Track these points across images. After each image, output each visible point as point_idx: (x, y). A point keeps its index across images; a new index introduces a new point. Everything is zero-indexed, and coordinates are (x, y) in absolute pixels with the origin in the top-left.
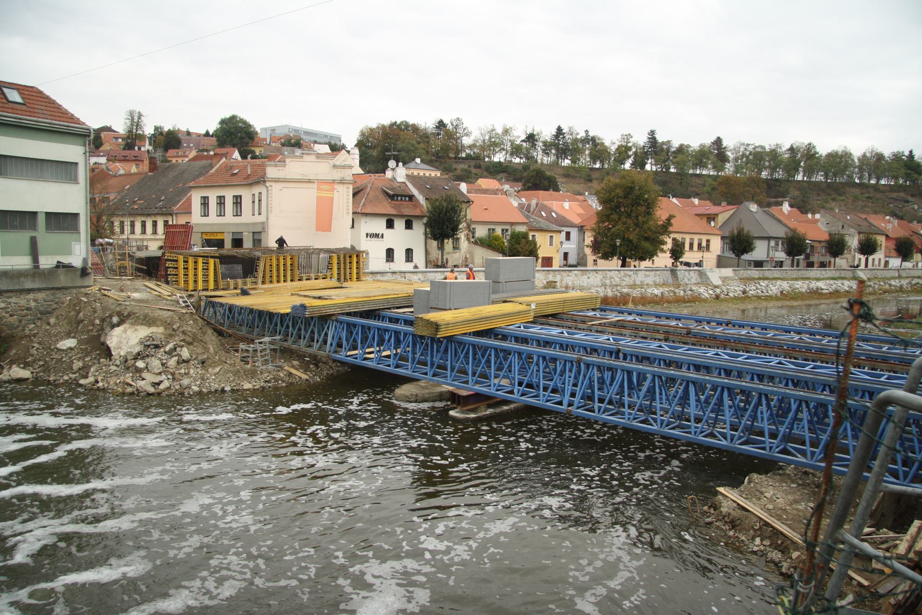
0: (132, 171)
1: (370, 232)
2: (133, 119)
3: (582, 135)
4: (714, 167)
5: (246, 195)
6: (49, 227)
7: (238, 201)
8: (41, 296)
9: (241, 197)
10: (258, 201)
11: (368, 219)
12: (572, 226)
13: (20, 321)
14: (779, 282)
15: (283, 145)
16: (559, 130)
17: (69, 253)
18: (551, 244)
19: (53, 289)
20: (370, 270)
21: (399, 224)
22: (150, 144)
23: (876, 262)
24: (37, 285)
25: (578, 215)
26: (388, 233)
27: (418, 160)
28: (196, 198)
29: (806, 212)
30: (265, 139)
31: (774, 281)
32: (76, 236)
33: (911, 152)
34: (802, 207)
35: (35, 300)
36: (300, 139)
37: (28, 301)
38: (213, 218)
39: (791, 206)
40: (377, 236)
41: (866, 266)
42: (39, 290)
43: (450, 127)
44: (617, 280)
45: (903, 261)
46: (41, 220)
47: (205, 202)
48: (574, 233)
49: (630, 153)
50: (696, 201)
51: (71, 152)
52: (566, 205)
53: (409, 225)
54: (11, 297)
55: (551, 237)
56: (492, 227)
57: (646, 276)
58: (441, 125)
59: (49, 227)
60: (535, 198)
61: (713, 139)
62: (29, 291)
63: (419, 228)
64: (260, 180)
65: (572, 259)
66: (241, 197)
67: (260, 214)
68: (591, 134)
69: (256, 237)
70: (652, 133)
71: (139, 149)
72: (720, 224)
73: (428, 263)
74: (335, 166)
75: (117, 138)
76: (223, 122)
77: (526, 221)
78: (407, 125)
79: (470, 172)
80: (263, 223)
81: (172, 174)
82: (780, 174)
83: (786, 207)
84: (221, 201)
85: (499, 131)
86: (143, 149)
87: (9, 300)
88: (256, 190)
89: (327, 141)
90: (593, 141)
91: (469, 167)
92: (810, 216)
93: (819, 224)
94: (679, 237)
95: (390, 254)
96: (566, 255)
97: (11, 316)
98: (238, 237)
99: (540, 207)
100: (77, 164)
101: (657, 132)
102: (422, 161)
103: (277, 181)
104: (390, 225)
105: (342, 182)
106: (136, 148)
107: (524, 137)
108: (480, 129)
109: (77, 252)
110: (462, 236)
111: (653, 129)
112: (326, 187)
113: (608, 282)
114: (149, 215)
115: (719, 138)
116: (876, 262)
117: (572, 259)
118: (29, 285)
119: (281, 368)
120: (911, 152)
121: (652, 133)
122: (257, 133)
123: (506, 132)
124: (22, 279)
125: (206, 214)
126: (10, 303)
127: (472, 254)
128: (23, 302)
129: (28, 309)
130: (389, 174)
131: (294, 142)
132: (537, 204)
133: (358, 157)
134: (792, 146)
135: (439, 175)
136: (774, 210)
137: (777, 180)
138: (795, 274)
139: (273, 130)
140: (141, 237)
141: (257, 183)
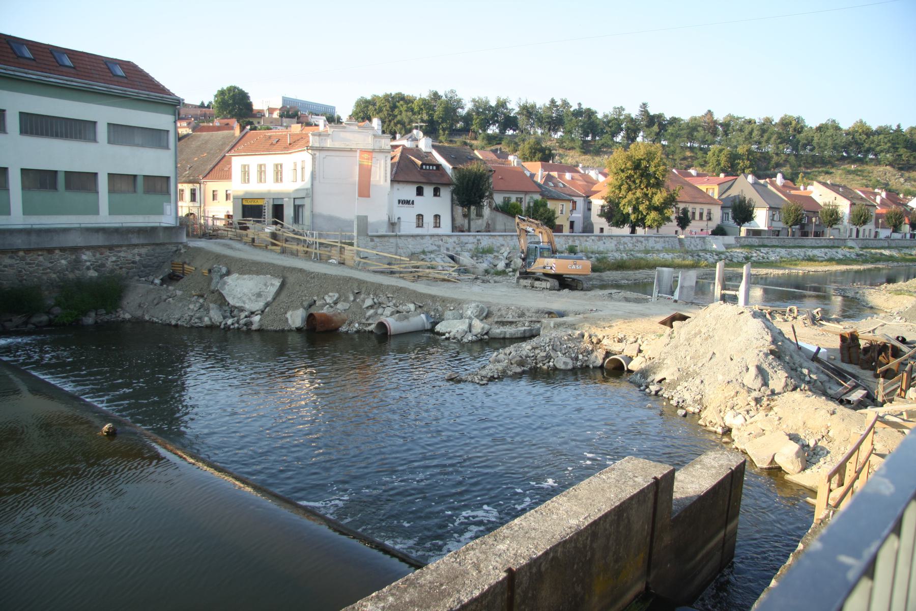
1: (402, 198)
3: (575, 107)
6: (69, 186)
8: (143, 251)
14: (778, 250)
16: (553, 102)
17: (161, 212)
19: (153, 244)
20: (402, 233)
21: (428, 191)
23: (867, 233)
24: (141, 241)
26: (418, 199)
31: (774, 249)
32: (90, 196)
33: (899, 126)
35: (140, 255)
37: (134, 255)
39: (784, 177)
40: (408, 202)
41: (857, 235)
42: (143, 245)
44: (630, 245)
45: (894, 231)
51: (160, 120)
53: (436, 193)
54: (120, 252)
56: (507, 195)
57: (656, 242)
58: (436, 96)
59: (69, 186)
61: (705, 111)
62: (136, 245)
63: (446, 194)
65: (578, 226)
68: (584, 107)
69: (298, 202)
70: (645, 105)
73: (454, 228)
83: (779, 180)
84: (261, 170)
85: (493, 103)
87: (119, 254)
90: (590, 113)
95: (420, 217)
96: (572, 224)
98: (279, 203)
100: (168, 131)
101: (649, 105)
104: (420, 192)
107: (517, 109)
108: (474, 101)
109: (168, 212)
110: (485, 202)
111: (644, 102)
112: (366, 156)
113: (622, 247)
115: (709, 111)
116: (867, 233)
117: (578, 226)
118: (135, 241)
119: (208, 310)
120: (899, 126)
121: (645, 105)
127: (494, 220)
128: (130, 257)
129: (134, 262)
138: (792, 242)
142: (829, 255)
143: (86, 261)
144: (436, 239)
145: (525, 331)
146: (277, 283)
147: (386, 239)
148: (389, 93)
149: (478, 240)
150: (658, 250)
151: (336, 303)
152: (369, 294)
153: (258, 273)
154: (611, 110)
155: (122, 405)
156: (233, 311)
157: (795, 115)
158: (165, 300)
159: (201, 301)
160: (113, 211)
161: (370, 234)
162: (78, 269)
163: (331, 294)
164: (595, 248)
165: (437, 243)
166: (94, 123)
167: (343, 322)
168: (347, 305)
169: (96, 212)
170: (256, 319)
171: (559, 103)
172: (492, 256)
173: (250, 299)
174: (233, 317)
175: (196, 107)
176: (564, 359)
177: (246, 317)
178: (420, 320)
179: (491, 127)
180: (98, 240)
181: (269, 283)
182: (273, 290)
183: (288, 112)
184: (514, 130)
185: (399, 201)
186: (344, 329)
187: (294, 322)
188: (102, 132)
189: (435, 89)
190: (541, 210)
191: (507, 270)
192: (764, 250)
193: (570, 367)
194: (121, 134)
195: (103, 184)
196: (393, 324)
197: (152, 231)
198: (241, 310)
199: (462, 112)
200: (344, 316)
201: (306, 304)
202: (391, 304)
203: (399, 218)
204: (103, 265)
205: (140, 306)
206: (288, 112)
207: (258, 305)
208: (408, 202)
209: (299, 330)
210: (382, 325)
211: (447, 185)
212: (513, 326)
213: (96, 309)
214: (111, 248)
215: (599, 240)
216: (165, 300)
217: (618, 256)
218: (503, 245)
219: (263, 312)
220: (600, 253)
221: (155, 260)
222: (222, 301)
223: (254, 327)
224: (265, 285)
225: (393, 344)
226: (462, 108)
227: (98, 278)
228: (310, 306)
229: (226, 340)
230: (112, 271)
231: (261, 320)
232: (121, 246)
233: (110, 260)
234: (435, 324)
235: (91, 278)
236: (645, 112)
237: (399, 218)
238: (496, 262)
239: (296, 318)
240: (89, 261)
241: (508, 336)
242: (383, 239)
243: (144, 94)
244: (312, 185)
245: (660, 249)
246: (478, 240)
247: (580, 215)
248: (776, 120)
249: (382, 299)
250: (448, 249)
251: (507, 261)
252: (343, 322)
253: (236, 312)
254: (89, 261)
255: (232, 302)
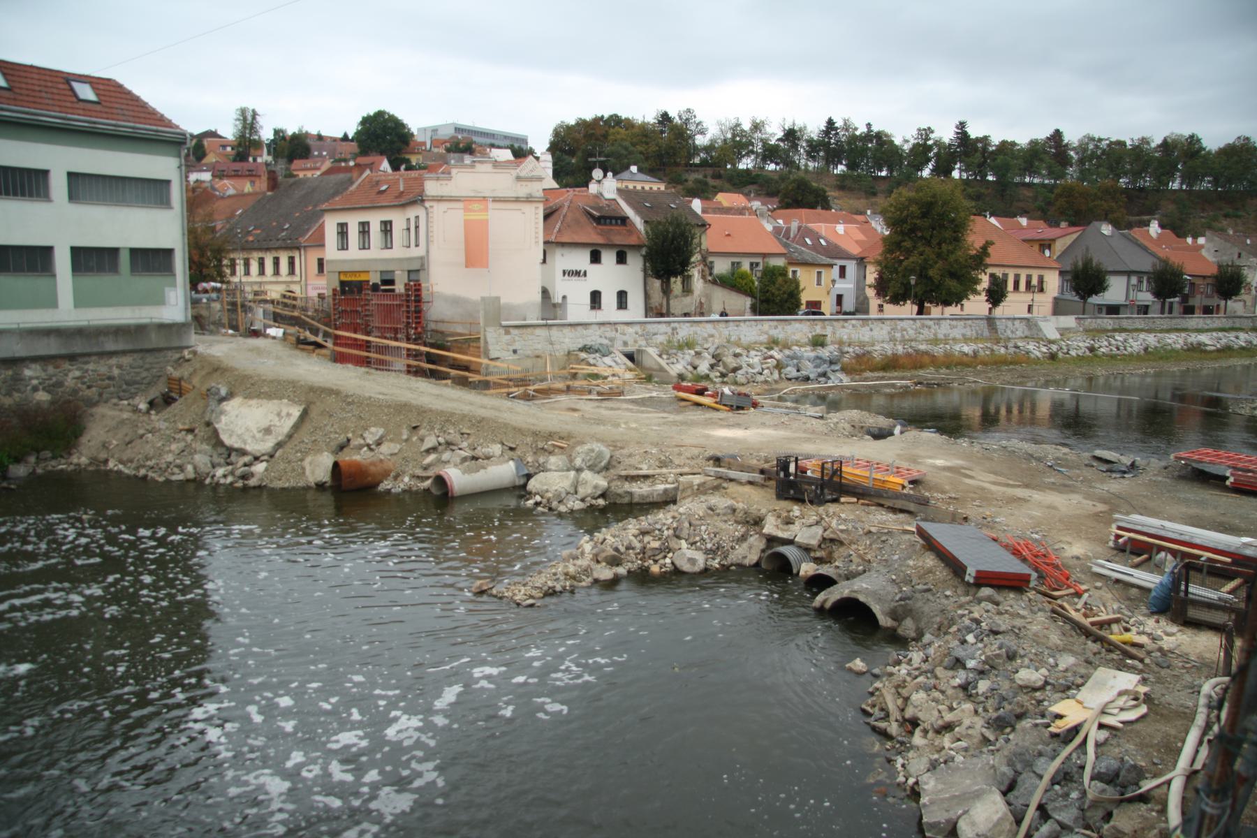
0: (246, 190)
2: (245, 119)
3: (862, 130)
4: (1051, 174)
5: (399, 219)
6: (134, 268)
7: (387, 227)
8: (126, 360)
9: (391, 222)
10: (413, 229)
11: (565, 251)
12: (849, 257)
13: (101, 395)
14: (1142, 336)
15: (448, 150)
16: (830, 123)
17: (160, 301)
18: (819, 283)
21: (608, 257)
22: (269, 154)
24: (120, 346)
25: (857, 242)
26: (593, 269)
27: (634, 169)
28: (330, 225)
29: (1185, 236)
30: (424, 143)
31: (1135, 334)
34: (1177, 227)
35: (120, 367)
36: (473, 142)
37: (110, 367)
38: (354, 252)
39: (1162, 226)
40: (577, 273)
42: (124, 353)
43: (677, 120)
44: (911, 332)
46: (124, 259)
47: (343, 230)
48: (851, 267)
49: (931, 154)
50: (1024, 221)
51: (162, 166)
52: (840, 229)
53: (621, 259)
55: (819, 273)
56: (736, 260)
57: (952, 327)
58: (665, 118)
59: (134, 268)
60: (795, 220)
63: (635, 263)
64: (418, 199)
65: (849, 304)
66: (391, 222)
67: (417, 245)
68: (875, 129)
70: (962, 125)
71: (255, 160)
72: (1058, 254)
73: (650, 310)
74: (519, 178)
75: (224, 147)
76: (366, 121)
77: (784, 251)
78: (616, 121)
79: (706, 184)
80: (422, 258)
81: (298, 194)
82: (1147, 182)
83: (1154, 228)
84: (364, 229)
85: (746, 126)
86: (259, 160)
87: (86, 367)
88: (412, 213)
89: (508, 143)
91: (705, 176)
92: (1189, 240)
93: (1204, 252)
94: (999, 272)
95: (596, 298)
97: (89, 387)
99: (804, 232)
101: (968, 124)
102: (640, 170)
103: (440, 199)
105: (529, 199)
106: (251, 159)
107: (780, 134)
111: (962, 119)
113: (898, 335)
114: (268, 249)
117: (849, 304)
118: (110, 346)
121: (962, 125)
122: (412, 135)
123: (757, 127)
124: (102, 338)
125: (344, 246)
126: (87, 371)
127: (708, 297)
128: (103, 369)
129: (110, 378)
130: (593, 188)
131: (464, 145)
132: (799, 228)
133: (550, 165)
134: (1165, 141)
135: (663, 188)
136: (1136, 232)
137: (1142, 190)
138: (1166, 324)
139: (435, 130)
140: (259, 279)
141: (413, 203)
142: (1224, 341)
143: (31, 378)
144: (608, 328)
145: (666, 491)
146: (296, 412)
147: (529, 330)
148: (599, 115)
149: (674, 329)
150: (954, 339)
151: (379, 443)
152: (432, 428)
153: (269, 396)
154: (915, 133)
155: (893, 386)
156: (230, 452)
157: (1186, 133)
158: (142, 436)
159: (190, 437)
160: (79, 302)
161: (504, 323)
162: (18, 391)
163: (373, 429)
164: (855, 337)
165: (608, 335)
166: (45, 173)
167: (386, 474)
168: (395, 447)
169: (53, 303)
170: (260, 468)
171: (839, 123)
172: (692, 352)
173: (254, 437)
174: (228, 464)
175: (335, 140)
176: (691, 553)
177: (245, 465)
178: (502, 471)
179: (744, 160)
180: (51, 347)
181: (284, 414)
182: (287, 425)
183: (458, 144)
184: (777, 164)
185: (564, 272)
186: (386, 485)
187: (313, 473)
188: (58, 185)
189: (663, 108)
190: (780, 279)
191: (712, 375)
192: (1119, 337)
193: (700, 565)
194: (84, 186)
195: (63, 262)
196: (458, 478)
197: (139, 330)
198: (243, 452)
199: (701, 141)
200: (390, 465)
201: (334, 444)
202: (465, 444)
203: (564, 297)
204: (60, 384)
205: (104, 446)
206: (458, 144)
207: (268, 445)
208: (577, 273)
209: (320, 486)
210: (440, 481)
211: (636, 248)
212: (648, 482)
213: (38, 451)
214: (72, 358)
215: (863, 326)
216: (142, 436)
217: (889, 349)
218: (712, 336)
219: (272, 456)
220: (862, 344)
221: (144, 374)
222: (216, 440)
223: (253, 482)
224: (279, 414)
225: (456, 514)
226: (702, 133)
227: (52, 403)
228: (342, 448)
229: (244, 498)
230: (75, 392)
231: (266, 470)
232: (89, 355)
233: (71, 375)
234: (529, 477)
235: (38, 403)
236: (963, 135)
237: (564, 297)
238: (697, 362)
239: (318, 468)
240: (37, 378)
241: (636, 500)
242: (525, 330)
243: (126, 125)
244: (428, 252)
245: (959, 336)
246: (674, 329)
247: (851, 286)
248: (1157, 141)
249: (453, 435)
250: (625, 344)
251: (713, 361)
252: (386, 474)
253: (233, 458)
254: (37, 378)
255: (228, 440)
